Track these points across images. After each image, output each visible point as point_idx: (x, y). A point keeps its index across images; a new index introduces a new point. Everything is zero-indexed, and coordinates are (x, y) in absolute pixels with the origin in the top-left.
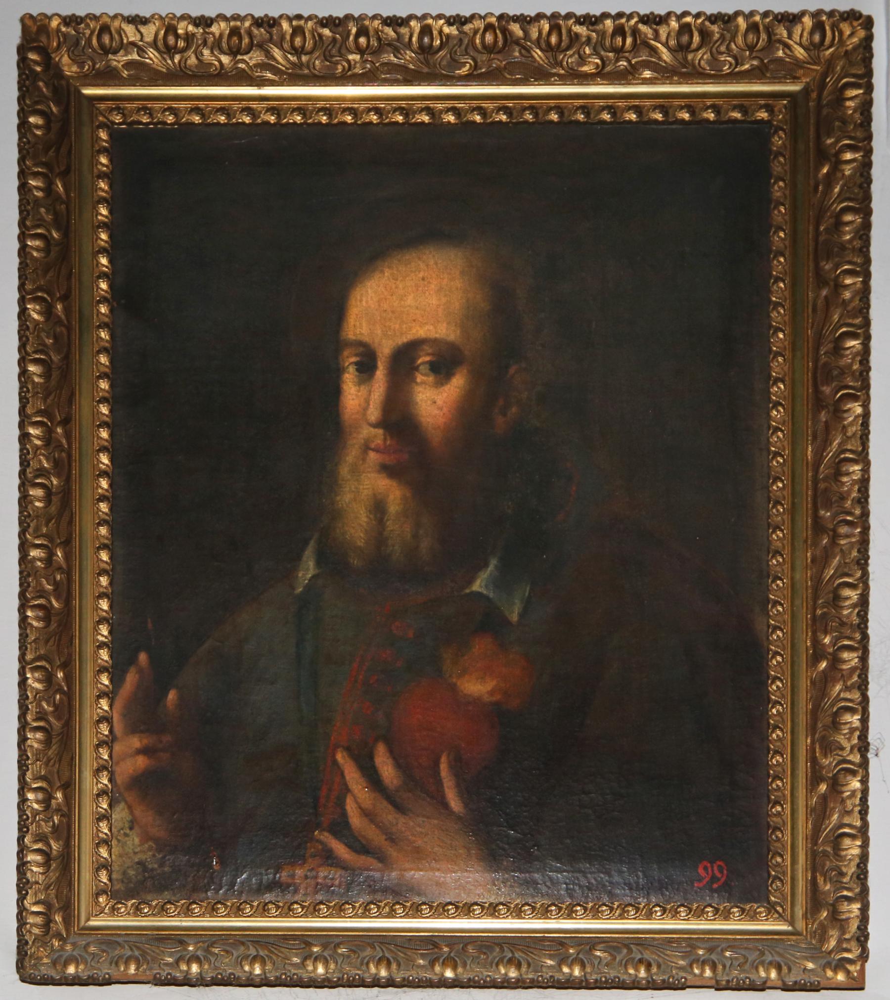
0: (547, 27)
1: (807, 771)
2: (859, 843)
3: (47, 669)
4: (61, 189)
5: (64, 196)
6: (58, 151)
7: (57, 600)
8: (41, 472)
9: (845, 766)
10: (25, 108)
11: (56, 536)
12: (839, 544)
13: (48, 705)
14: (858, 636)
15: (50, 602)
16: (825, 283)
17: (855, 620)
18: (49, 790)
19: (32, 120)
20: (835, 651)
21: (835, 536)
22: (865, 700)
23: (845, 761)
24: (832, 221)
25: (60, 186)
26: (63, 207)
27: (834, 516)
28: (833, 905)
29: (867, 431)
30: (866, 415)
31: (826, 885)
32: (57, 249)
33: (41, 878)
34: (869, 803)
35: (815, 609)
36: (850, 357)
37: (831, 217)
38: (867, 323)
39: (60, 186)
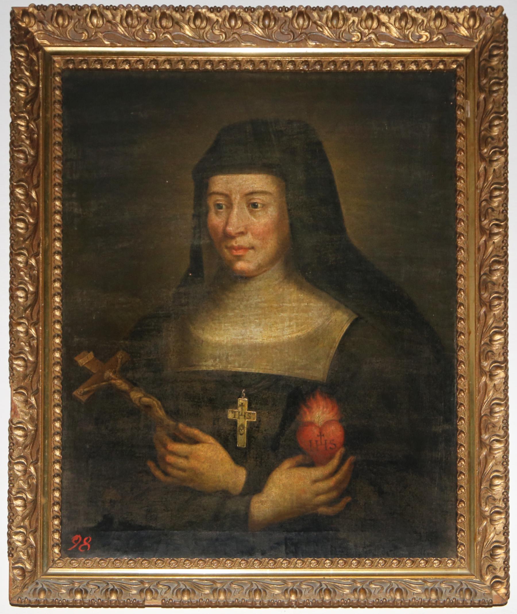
0: (331, 14)
1: (475, 179)
2: (503, 516)
3: (23, 533)
4: (33, 541)
5: (35, 335)
6: (32, 311)
7: (32, 356)
8: (21, 490)
9: (497, 580)
10: (13, 251)
11: (30, 457)
12: (493, 454)
13: (24, 554)
14: (502, 469)
15: (27, 357)
16: (485, 518)
17: (501, 281)
18: (26, 463)
19: (18, 88)
20: (491, 515)
21: (491, 449)
22: (507, 471)
23: (497, 577)
24: (487, 124)
25: (32, 539)
26: (36, 203)
27: (490, 438)
28: (490, 371)
29: (506, 171)
30: (506, 378)
31: (486, 507)
32: (29, 574)
33: (21, 439)
34: (509, 385)
35: (480, 133)
36: (498, 418)
37: (487, 481)
38: (506, 326)
39: (32, 539)
